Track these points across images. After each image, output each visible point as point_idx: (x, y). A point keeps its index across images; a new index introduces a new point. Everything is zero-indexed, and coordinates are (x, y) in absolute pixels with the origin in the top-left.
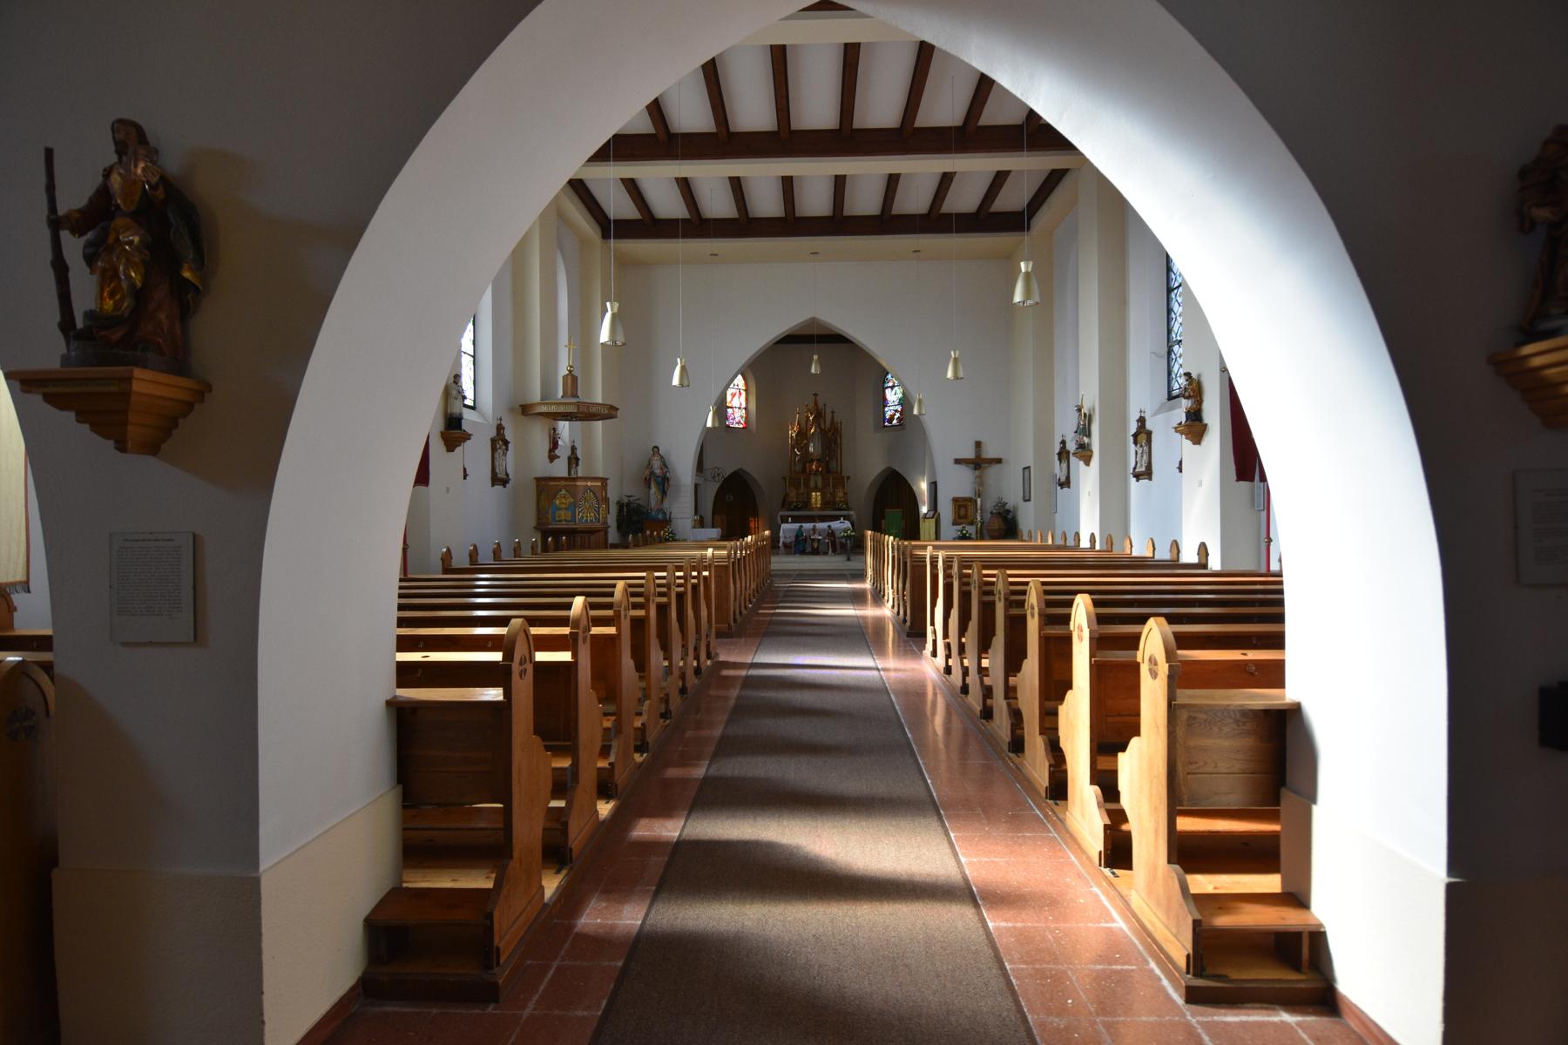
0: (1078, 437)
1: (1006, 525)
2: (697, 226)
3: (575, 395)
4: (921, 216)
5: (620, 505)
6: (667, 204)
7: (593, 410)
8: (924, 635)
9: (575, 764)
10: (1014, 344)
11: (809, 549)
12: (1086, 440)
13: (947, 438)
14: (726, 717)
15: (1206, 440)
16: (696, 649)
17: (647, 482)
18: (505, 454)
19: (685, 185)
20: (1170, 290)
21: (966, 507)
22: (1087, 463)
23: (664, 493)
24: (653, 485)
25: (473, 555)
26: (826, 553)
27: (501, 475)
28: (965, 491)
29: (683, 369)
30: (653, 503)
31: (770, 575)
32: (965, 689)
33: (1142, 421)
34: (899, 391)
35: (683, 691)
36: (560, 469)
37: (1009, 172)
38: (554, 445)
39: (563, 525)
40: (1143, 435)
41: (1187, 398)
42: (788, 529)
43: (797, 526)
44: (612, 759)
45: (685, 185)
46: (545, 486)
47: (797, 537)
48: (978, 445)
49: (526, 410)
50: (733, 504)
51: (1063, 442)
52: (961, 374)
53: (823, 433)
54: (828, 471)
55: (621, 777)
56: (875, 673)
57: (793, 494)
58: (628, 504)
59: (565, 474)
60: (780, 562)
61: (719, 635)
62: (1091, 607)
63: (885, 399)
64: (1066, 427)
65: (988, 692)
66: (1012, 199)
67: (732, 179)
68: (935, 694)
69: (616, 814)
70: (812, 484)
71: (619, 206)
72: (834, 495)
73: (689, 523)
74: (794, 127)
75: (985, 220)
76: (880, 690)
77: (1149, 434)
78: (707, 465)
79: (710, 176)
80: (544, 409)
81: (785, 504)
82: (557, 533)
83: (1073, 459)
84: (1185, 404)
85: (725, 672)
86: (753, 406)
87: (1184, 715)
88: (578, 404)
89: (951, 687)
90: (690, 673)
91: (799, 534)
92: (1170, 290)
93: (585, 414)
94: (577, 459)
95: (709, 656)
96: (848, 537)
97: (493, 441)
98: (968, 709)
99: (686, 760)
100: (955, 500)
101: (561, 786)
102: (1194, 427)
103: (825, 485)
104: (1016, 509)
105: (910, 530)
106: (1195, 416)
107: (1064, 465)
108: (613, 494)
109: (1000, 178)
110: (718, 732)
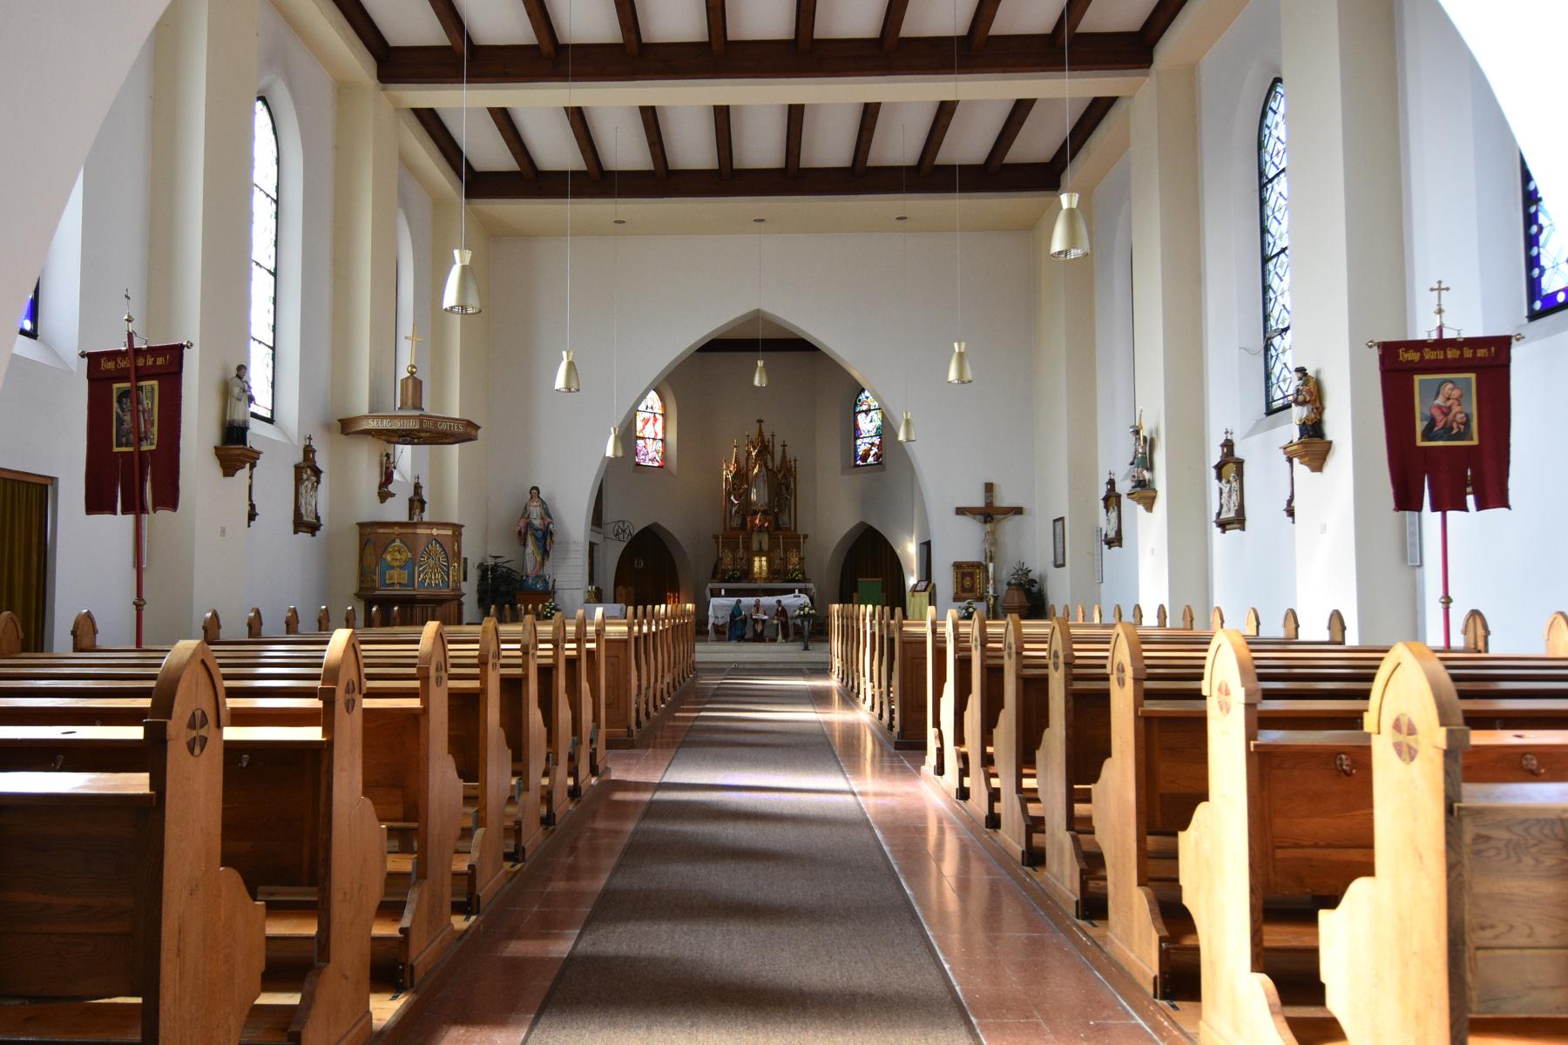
0: (1135, 471)
1: (1031, 600)
2: (595, 180)
3: (418, 406)
4: (908, 168)
5: (483, 568)
6: (555, 149)
7: (443, 427)
8: (922, 747)
9: (325, 929)
10: (1043, 322)
11: (749, 634)
12: (1147, 475)
13: (944, 480)
14: (613, 861)
15: (1332, 463)
16: (572, 758)
17: (522, 537)
18: (315, 488)
19: (578, 118)
20: (1265, 260)
21: (972, 575)
22: (1149, 507)
23: (545, 553)
24: (530, 540)
25: (255, 625)
26: (774, 640)
27: (308, 518)
28: (972, 554)
29: (571, 365)
30: (530, 566)
31: (694, 668)
32: (993, 821)
33: (1228, 445)
34: (876, 417)
35: (548, 820)
36: (396, 510)
37: (1033, 101)
38: (387, 478)
39: (397, 591)
40: (1230, 464)
41: (1303, 403)
42: (720, 607)
43: (732, 601)
44: (406, 922)
45: (578, 118)
46: (371, 535)
47: (733, 616)
48: (989, 488)
49: (347, 426)
50: (644, 567)
51: (1111, 483)
52: (968, 375)
53: (770, 473)
54: (778, 528)
55: (422, 955)
56: (850, 798)
57: (728, 559)
58: (495, 567)
59: (404, 518)
60: (708, 652)
61: (611, 744)
62: (1244, 650)
63: (856, 428)
64: (1116, 462)
65: (1035, 825)
66: (1034, 145)
67: (643, 110)
68: (941, 831)
69: (405, 1021)
70: (755, 546)
71: (489, 152)
72: (785, 560)
73: (580, 596)
74: (731, 36)
75: (998, 174)
76: (860, 823)
77: (1240, 464)
78: (609, 515)
79: (614, 104)
80: (372, 424)
81: (717, 573)
82: (386, 603)
83: (1126, 503)
84: (1298, 413)
85: (619, 796)
86: (672, 437)
87: (1469, 830)
88: (421, 418)
89: (969, 821)
90: (560, 797)
91: (736, 611)
92: (1265, 260)
93: (433, 434)
94: (423, 503)
95: (594, 771)
96: (805, 616)
97: (298, 469)
98: (1001, 855)
99: (548, 927)
100: (958, 566)
101: (287, 966)
102: (1313, 445)
103: (774, 546)
104: (1043, 578)
105: (894, 596)
106: (1313, 431)
107: (1113, 515)
108: (473, 550)
109: (1021, 109)
110: (600, 883)
